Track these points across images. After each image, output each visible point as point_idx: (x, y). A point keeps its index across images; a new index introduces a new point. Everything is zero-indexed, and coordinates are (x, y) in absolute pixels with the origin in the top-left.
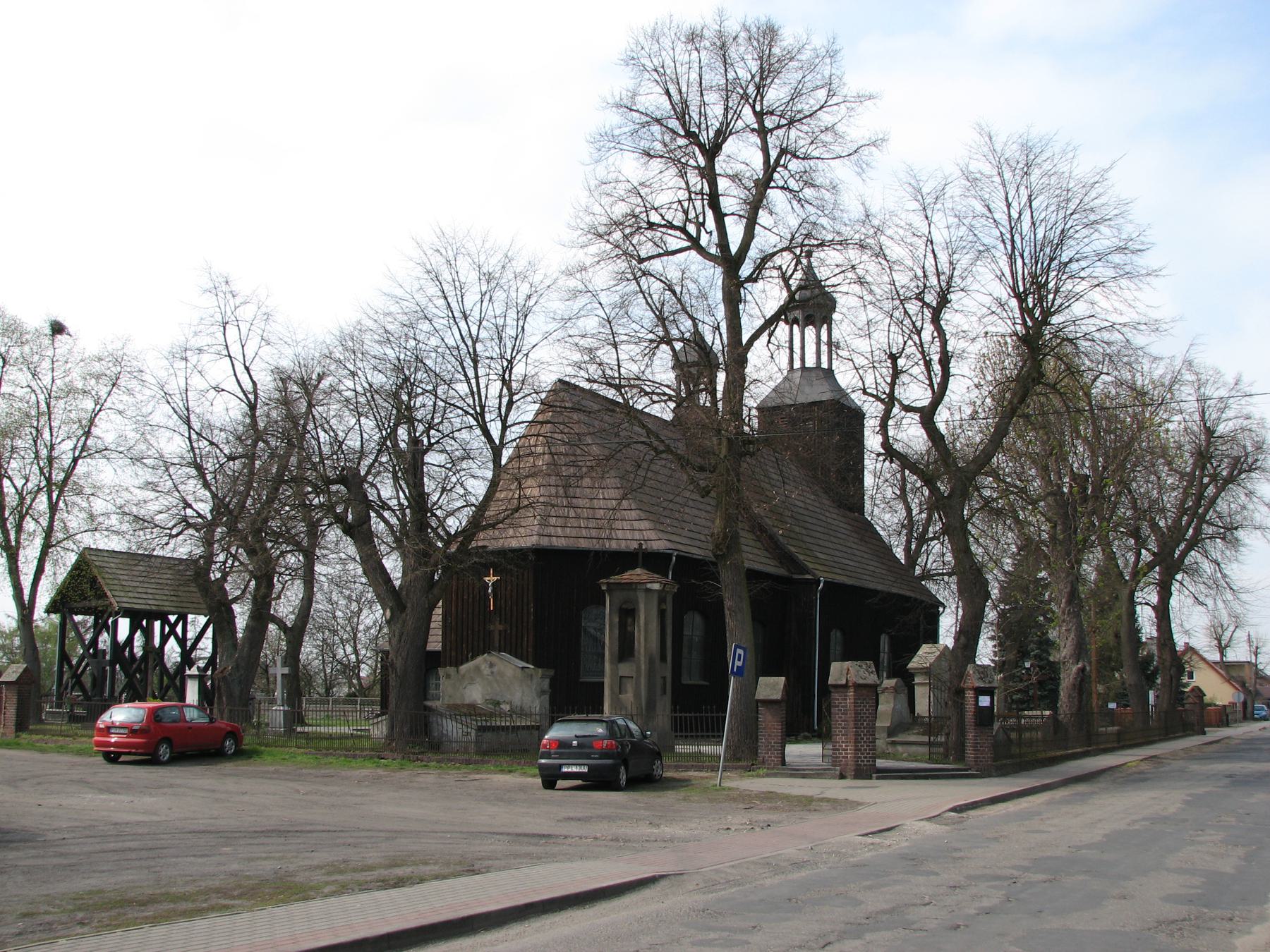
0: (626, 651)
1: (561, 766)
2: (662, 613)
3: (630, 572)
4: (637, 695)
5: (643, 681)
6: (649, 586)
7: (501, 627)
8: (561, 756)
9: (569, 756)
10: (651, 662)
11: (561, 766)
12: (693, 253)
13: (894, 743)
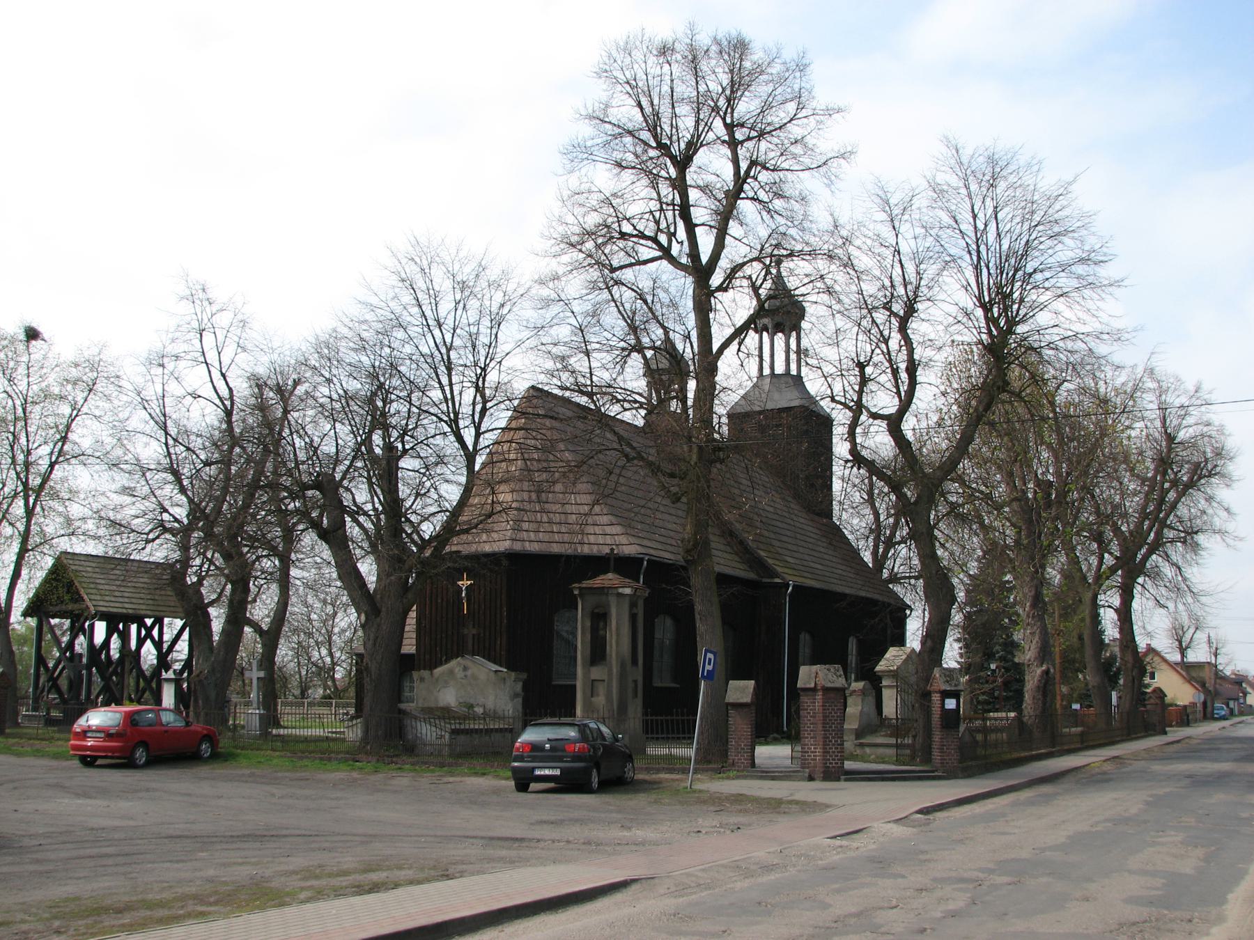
0: (598, 654)
1: (533, 769)
3: (602, 577)
6: (620, 590)
7: (474, 631)
8: (534, 759)
9: (542, 760)
11: (533, 769)
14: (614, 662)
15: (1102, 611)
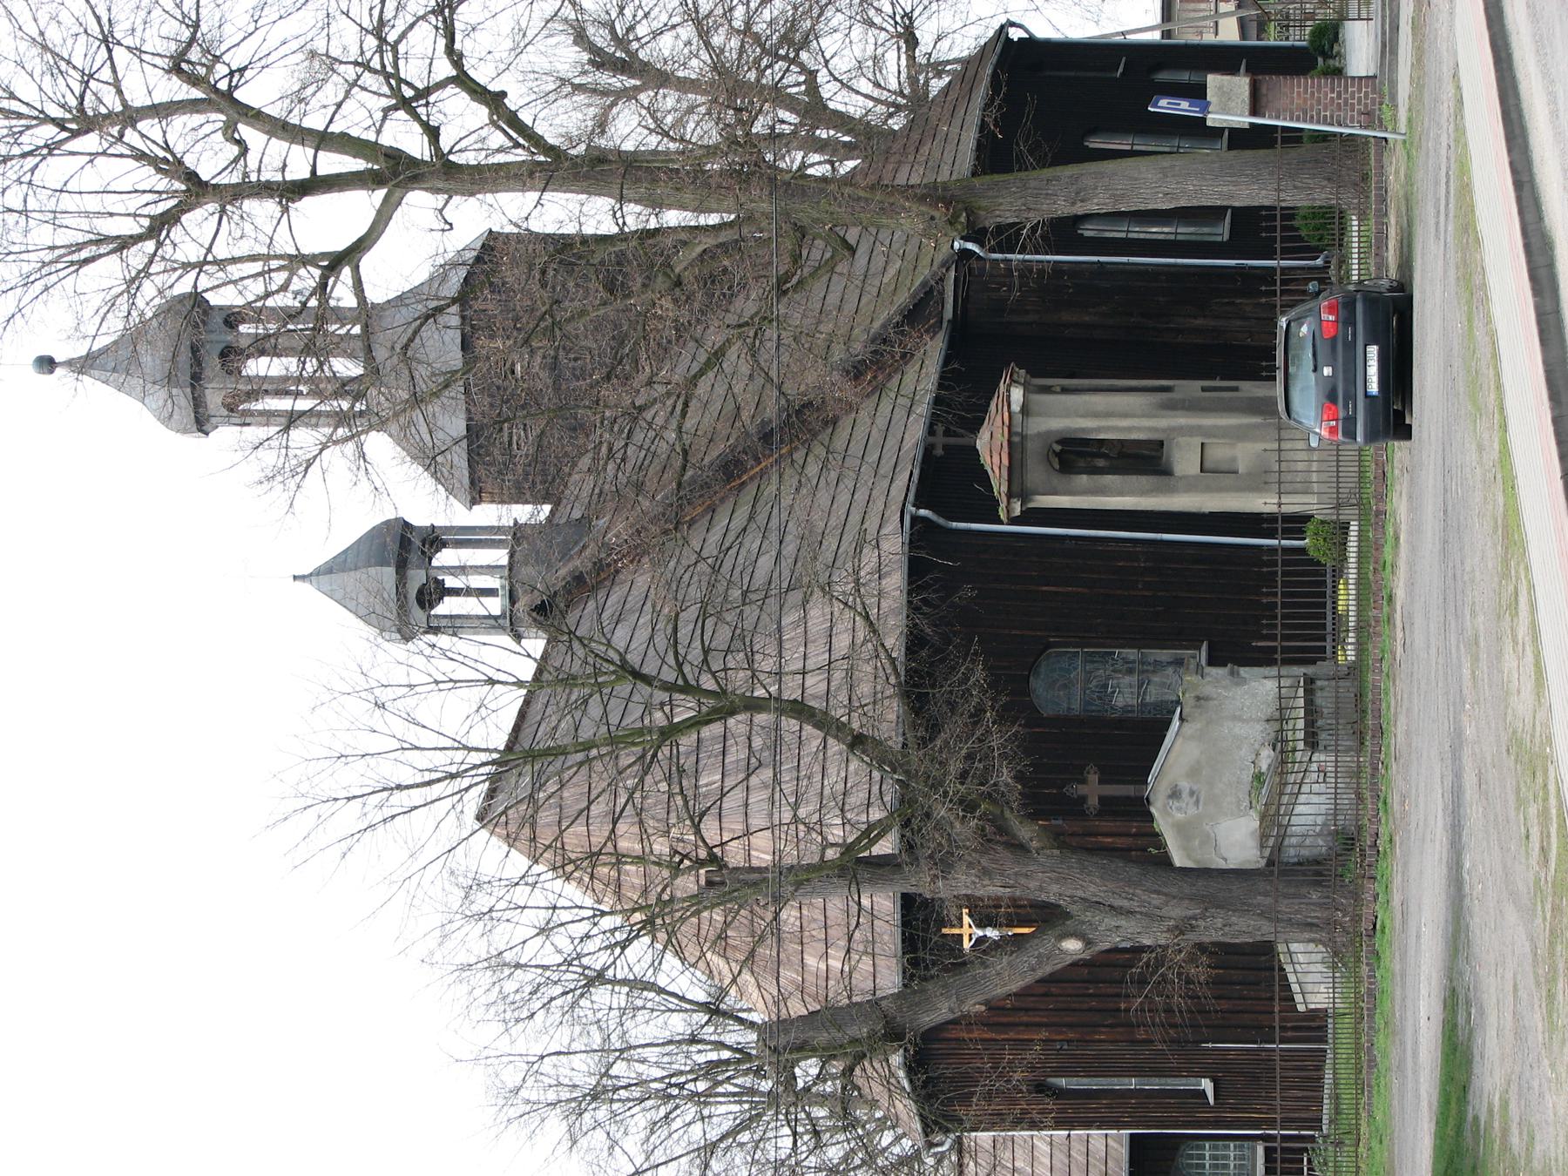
0: (1146, 459)
1: (1366, 395)
2: (1065, 390)
3: (985, 458)
4: (1239, 435)
6: (1016, 407)
7: (1093, 778)
8: (1350, 397)
10: (1171, 406)
11: (1366, 395)
12: (367, 263)
13: (1349, 305)
15: (288, 178)
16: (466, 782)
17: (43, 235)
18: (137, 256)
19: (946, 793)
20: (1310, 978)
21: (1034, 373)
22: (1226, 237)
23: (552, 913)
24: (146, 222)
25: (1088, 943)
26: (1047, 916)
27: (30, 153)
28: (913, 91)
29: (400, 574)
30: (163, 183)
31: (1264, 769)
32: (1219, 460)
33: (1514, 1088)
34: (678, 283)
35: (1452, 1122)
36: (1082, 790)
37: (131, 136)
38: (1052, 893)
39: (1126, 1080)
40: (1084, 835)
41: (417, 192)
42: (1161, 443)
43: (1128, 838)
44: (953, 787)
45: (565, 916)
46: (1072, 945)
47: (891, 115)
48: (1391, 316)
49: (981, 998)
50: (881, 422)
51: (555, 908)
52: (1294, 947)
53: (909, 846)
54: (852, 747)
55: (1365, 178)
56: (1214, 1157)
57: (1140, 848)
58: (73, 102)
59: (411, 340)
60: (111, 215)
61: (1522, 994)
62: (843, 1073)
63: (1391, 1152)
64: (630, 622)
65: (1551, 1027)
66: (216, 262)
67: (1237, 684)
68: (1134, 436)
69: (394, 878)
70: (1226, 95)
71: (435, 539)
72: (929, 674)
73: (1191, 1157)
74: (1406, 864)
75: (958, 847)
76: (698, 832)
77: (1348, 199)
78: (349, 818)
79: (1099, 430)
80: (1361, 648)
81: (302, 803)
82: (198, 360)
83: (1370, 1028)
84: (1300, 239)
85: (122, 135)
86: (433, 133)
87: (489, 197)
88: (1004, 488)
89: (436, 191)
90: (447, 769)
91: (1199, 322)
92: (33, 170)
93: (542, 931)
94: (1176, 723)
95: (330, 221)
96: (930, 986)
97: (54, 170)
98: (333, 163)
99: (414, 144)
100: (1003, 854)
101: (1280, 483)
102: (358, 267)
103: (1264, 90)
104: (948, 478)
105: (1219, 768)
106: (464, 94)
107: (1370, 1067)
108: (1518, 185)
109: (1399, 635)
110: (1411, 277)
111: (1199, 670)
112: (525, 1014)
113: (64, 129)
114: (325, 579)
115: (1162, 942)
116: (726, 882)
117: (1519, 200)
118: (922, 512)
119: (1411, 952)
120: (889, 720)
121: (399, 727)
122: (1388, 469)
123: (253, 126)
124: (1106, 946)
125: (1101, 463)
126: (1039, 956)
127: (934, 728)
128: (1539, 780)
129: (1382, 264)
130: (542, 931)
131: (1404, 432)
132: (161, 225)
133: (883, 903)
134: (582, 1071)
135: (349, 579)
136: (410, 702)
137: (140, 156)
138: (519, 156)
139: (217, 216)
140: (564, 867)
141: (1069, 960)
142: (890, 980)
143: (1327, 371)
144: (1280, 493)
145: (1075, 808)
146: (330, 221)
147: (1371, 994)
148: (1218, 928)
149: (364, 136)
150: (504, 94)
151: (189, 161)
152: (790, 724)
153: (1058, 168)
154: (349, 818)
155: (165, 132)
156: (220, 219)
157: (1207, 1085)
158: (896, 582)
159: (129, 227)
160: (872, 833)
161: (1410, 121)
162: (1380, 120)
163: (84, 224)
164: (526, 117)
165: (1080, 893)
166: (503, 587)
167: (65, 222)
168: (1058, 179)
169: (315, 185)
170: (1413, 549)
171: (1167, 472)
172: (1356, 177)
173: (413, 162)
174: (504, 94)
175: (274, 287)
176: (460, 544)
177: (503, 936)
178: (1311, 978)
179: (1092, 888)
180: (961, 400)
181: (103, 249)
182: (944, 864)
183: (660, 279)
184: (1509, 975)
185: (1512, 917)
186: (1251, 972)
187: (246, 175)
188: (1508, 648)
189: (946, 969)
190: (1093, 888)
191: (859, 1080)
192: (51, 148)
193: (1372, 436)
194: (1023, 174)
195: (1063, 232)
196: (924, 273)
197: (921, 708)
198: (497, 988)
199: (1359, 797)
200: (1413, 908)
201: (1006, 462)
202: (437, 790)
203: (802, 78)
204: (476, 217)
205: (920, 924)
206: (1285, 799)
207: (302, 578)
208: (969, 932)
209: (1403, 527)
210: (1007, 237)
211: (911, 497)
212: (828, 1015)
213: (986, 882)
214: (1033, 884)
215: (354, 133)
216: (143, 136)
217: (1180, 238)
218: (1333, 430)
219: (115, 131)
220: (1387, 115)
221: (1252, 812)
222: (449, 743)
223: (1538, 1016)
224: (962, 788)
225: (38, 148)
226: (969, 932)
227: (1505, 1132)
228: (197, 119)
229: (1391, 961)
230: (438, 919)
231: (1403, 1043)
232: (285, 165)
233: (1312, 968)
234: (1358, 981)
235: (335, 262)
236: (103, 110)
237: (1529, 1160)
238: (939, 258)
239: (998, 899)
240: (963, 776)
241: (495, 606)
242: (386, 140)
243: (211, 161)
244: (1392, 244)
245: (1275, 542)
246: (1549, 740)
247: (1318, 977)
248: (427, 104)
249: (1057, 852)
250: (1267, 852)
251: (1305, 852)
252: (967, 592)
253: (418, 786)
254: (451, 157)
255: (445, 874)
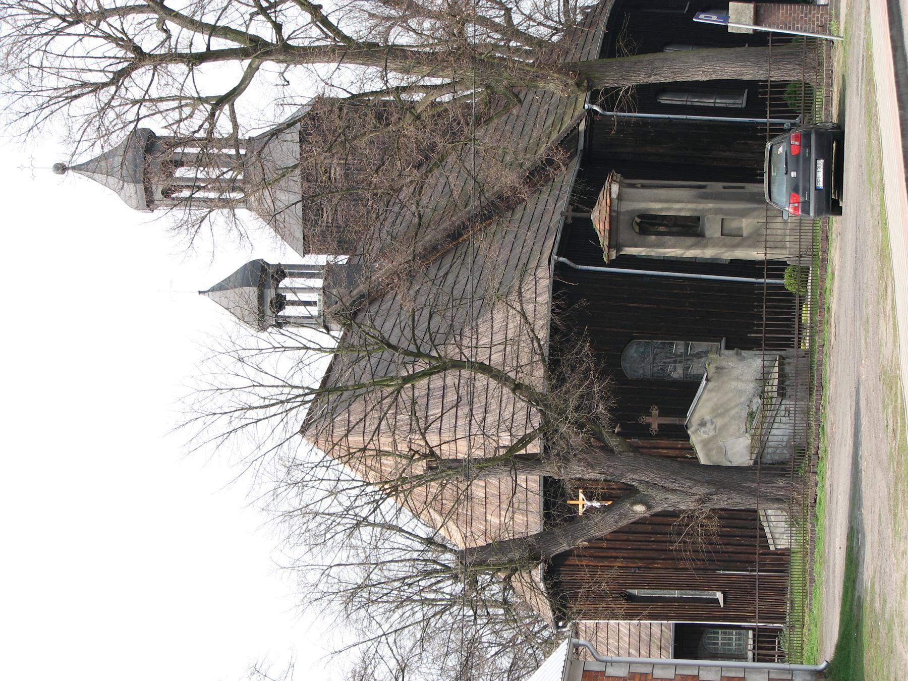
0: (689, 228)
1: (816, 189)
2: (643, 186)
4: (743, 214)
5: (726, 206)
6: (614, 196)
7: (655, 412)
8: (806, 190)
9: (807, 180)
11: (816, 189)
12: (239, 102)
14: (701, 206)
15: (193, 51)
16: (289, 406)
17: (51, 81)
18: (105, 95)
19: (567, 418)
20: (778, 530)
21: (626, 176)
22: (744, 105)
23: (338, 483)
24: (111, 76)
25: (649, 507)
26: (629, 493)
27: (46, 34)
28: (566, 21)
29: (261, 290)
30: (121, 53)
31: (754, 410)
32: (736, 232)
33: (878, 575)
34: (418, 117)
35: (848, 603)
36: (648, 420)
37: (103, 26)
38: (630, 478)
39: (672, 592)
40: (651, 448)
41: (268, 62)
42: (698, 218)
43: (671, 445)
44: (571, 415)
45: (345, 485)
46: (640, 508)
47: (553, 34)
48: (832, 143)
49: (585, 538)
50: (540, 207)
51: (339, 480)
52: (769, 512)
53: (546, 449)
54: (514, 391)
55: (820, 64)
56: (723, 639)
57: (685, 460)
58: (70, 5)
59: (263, 148)
60: (90, 70)
61: (883, 519)
62: (504, 580)
63: (821, 631)
64: (389, 321)
65: (896, 533)
66: (151, 100)
67: (740, 360)
68: (683, 214)
69: (247, 460)
70: (739, 13)
71: (281, 272)
72: (561, 350)
73: (710, 638)
74: (833, 464)
75: (572, 449)
76: (424, 438)
77: (811, 78)
78: (222, 424)
79: (662, 210)
80: (812, 341)
81: (195, 415)
82: (150, 167)
83: (812, 560)
84: (786, 105)
85: (98, 24)
86: (278, 27)
87: (310, 65)
88: (606, 243)
89: (279, 61)
90: (278, 397)
91: (727, 154)
92: (47, 44)
93: (331, 493)
94: (704, 382)
95: (217, 78)
96: (557, 531)
97: (60, 44)
98: (219, 43)
99: (266, 33)
100: (600, 454)
101: (766, 241)
102: (233, 104)
103: (762, 11)
104: (576, 239)
105: (726, 409)
106: (298, 7)
107: (811, 583)
108: (894, 49)
109: (833, 330)
110: (844, 121)
111: (718, 351)
112: (321, 540)
113: (64, 20)
114: (217, 294)
115: (692, 508)
116: (439, 467)
117: (894, 56)
118: (561, 259)
119: (834, 513)
120: (537, 377)
121: (252, 373)
122: (829, 234)
123: (173, 21)
124: (659, 509)
125: (662, 229)
126: (621, 514)
127: (562, 380)
128: (893, 391)
129: (829, 114)
130: (331, 493)
131: (838, 211)
132: (119, 77)
133: (531, 481)
134: (355, 576)
135: (231, 294)
136: (259, 358)
137: (107, 37)
138: (328, 42)
139: (151, 71)
140: (349, 457)
141: (637, 517)
142: (535, 526)
143: (793, 174)
144: (766, 248)
145: (644, 431)
146: (217, 78)
147: (812, 540)
148: (724, 501)
149: (239, 29)
150: (320, 7)
151: (137, 40)
152: (482, 380)
153: (641, 56)
154: (222, 424)
155: (122, 23)
156: (154, 74)
157: (719, 595)
158: (545, 298)
159: (100, 78)
160: (525, 441)
161: (846, 29)
162: (830, 30)
163: (74, 75)
164: (332, 19)
165: (645, 479)
166: (320, 300)
167: (63, 74)
168: (641, 62)
169: (209, 55)
170: (841, 278)
171: (701, 235)
172: (814, 64)
173: (266, 44)
174: (320, 7)
175: (184, 116)
176: (292, 275)
177: (309, 495)
178: (778, 529)
179: (652, 476)
180: (585, 195)
181: (85, 90)
182: (565, 459)
183: (408, 115)
184: (877, 510)
185: (879, 475)
186: (743, 527)
187: (170, 49)
188: (882, 315)
189: (565, 520)
190: (650, 477)
191: (516, 584)
192: (58, 32)
193: (818, 212)
194: (620, 59)
195: (647, 95)
196: (568, 122)
197: (555, 370)
198: (305, 526)
199: (809, 425)
200: (835, 487)
201: (607, 227)
202: (274, 410)
203: (502, 12)
204: (305, 84)
205: (554, 494)
206: (765, 426)
207: (204, 292)
208: (582, 503)
209: (837, 267)
210: (610, 98)
211: (555, 250)
212: (500, 546)
213: (590, 471)
214: (617, 473)
215: (233, 26)
216: (109, 25)
217: (717, 105)
218: (796, 209)
219: (94, 22)
220: (834, 28)
221: (747, 435)
222: (281, 383)
223: (890, 530)
224: (576, 415)
225: (51, 31)
226: (582, 503)
227: (872, 600)
228: (141, 17)
229: (823, 521)
230: (272, 486)
231: (829, 567)
232: (192, 43)
233: (780, 524)
234: (805, 532)
235: (221, 101)
236: (88, 11)
237: (883, 614)
238: (577, 113)
239: (596, 481)
240: (577, 409)
241: (314, 311)
242: (252, 31)
243: (150, 42)
244: (835, 102)
245: (768, 281)
246: (898, 366)
247: (783, 530)
248: (275, 11)
249: (631, 454)
250: (754, 457)
251: (776, 458)
252: (583, 302)
253: (261, 407)
254: (288, 42)
255: (276, 458)
